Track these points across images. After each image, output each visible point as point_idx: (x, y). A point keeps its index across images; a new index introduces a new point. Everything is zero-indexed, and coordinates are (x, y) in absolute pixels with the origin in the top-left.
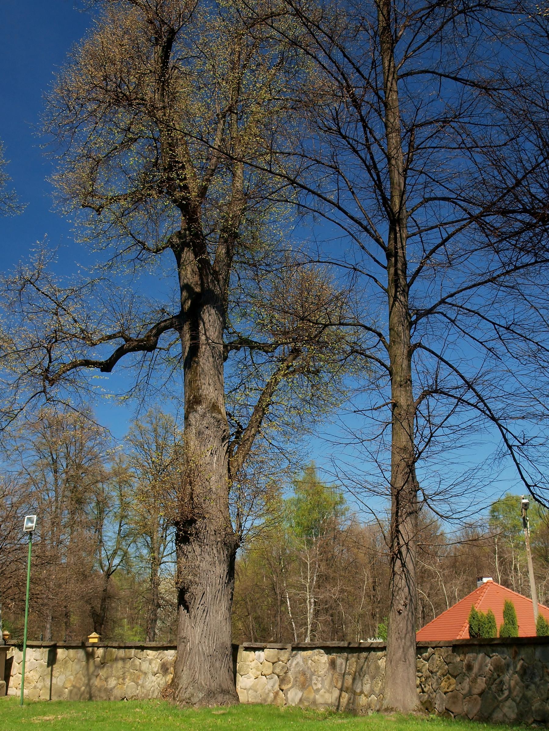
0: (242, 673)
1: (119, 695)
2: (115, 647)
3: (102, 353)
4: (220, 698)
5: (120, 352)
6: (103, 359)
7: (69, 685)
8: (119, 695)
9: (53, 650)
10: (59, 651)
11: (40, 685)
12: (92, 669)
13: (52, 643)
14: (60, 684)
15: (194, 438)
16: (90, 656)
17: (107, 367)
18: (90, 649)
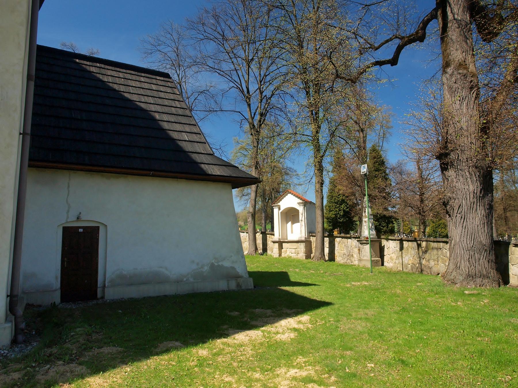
0: (513, 263)
1: (436, 272)
2: (431, 241)
3: (386, 53)
4: (479, 280)
5: (399, 49)
6: (390, 57)
7: (410, 262)
8: (436, 272)
9: (401, 241)
10: (404, 242)
11: (397, 261)
12: (421, 254)
13: (400, 238)
14: (406, 262)
15: (447, 93)
16: (419, 246)
17: (394, 62)
18: (419, 242)
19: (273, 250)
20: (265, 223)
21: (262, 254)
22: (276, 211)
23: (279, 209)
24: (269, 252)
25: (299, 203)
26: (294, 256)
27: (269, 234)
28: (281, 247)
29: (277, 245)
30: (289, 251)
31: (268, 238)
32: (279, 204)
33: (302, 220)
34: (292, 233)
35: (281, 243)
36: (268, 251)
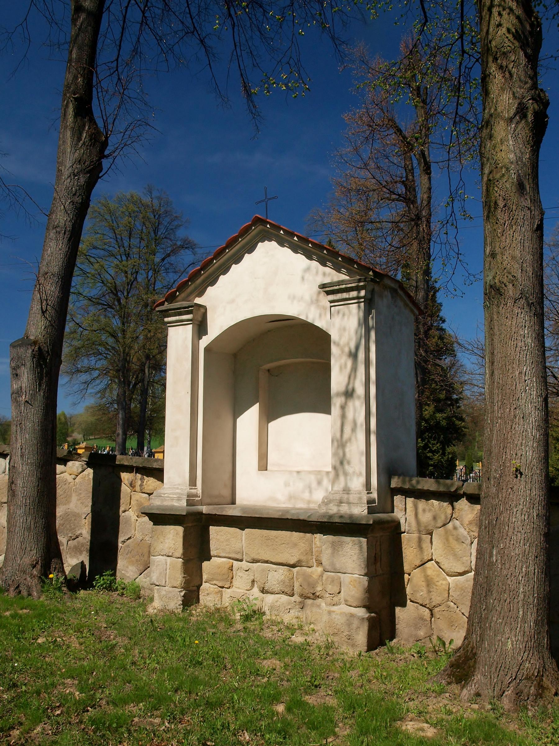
19: (153, 563)
20: (125, 433)
21: (81, 582)
22: (179, 339)
23: (201, 328)
24: (126, 569)
25: (327, 289)
26: (277, 607)
27: (129, 469)
28: (197, 550)
29: (173, 537)
30: (245, 578)
31: (125, 488)
32: (198, 301)
33: (349, 394)
34: (263, 465)
35: (196, 528)
36: (121, 563)
